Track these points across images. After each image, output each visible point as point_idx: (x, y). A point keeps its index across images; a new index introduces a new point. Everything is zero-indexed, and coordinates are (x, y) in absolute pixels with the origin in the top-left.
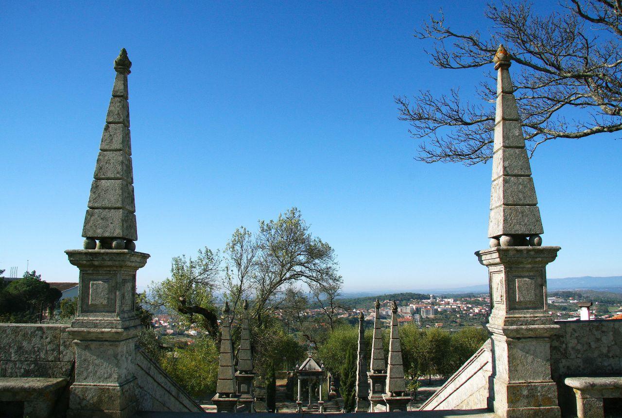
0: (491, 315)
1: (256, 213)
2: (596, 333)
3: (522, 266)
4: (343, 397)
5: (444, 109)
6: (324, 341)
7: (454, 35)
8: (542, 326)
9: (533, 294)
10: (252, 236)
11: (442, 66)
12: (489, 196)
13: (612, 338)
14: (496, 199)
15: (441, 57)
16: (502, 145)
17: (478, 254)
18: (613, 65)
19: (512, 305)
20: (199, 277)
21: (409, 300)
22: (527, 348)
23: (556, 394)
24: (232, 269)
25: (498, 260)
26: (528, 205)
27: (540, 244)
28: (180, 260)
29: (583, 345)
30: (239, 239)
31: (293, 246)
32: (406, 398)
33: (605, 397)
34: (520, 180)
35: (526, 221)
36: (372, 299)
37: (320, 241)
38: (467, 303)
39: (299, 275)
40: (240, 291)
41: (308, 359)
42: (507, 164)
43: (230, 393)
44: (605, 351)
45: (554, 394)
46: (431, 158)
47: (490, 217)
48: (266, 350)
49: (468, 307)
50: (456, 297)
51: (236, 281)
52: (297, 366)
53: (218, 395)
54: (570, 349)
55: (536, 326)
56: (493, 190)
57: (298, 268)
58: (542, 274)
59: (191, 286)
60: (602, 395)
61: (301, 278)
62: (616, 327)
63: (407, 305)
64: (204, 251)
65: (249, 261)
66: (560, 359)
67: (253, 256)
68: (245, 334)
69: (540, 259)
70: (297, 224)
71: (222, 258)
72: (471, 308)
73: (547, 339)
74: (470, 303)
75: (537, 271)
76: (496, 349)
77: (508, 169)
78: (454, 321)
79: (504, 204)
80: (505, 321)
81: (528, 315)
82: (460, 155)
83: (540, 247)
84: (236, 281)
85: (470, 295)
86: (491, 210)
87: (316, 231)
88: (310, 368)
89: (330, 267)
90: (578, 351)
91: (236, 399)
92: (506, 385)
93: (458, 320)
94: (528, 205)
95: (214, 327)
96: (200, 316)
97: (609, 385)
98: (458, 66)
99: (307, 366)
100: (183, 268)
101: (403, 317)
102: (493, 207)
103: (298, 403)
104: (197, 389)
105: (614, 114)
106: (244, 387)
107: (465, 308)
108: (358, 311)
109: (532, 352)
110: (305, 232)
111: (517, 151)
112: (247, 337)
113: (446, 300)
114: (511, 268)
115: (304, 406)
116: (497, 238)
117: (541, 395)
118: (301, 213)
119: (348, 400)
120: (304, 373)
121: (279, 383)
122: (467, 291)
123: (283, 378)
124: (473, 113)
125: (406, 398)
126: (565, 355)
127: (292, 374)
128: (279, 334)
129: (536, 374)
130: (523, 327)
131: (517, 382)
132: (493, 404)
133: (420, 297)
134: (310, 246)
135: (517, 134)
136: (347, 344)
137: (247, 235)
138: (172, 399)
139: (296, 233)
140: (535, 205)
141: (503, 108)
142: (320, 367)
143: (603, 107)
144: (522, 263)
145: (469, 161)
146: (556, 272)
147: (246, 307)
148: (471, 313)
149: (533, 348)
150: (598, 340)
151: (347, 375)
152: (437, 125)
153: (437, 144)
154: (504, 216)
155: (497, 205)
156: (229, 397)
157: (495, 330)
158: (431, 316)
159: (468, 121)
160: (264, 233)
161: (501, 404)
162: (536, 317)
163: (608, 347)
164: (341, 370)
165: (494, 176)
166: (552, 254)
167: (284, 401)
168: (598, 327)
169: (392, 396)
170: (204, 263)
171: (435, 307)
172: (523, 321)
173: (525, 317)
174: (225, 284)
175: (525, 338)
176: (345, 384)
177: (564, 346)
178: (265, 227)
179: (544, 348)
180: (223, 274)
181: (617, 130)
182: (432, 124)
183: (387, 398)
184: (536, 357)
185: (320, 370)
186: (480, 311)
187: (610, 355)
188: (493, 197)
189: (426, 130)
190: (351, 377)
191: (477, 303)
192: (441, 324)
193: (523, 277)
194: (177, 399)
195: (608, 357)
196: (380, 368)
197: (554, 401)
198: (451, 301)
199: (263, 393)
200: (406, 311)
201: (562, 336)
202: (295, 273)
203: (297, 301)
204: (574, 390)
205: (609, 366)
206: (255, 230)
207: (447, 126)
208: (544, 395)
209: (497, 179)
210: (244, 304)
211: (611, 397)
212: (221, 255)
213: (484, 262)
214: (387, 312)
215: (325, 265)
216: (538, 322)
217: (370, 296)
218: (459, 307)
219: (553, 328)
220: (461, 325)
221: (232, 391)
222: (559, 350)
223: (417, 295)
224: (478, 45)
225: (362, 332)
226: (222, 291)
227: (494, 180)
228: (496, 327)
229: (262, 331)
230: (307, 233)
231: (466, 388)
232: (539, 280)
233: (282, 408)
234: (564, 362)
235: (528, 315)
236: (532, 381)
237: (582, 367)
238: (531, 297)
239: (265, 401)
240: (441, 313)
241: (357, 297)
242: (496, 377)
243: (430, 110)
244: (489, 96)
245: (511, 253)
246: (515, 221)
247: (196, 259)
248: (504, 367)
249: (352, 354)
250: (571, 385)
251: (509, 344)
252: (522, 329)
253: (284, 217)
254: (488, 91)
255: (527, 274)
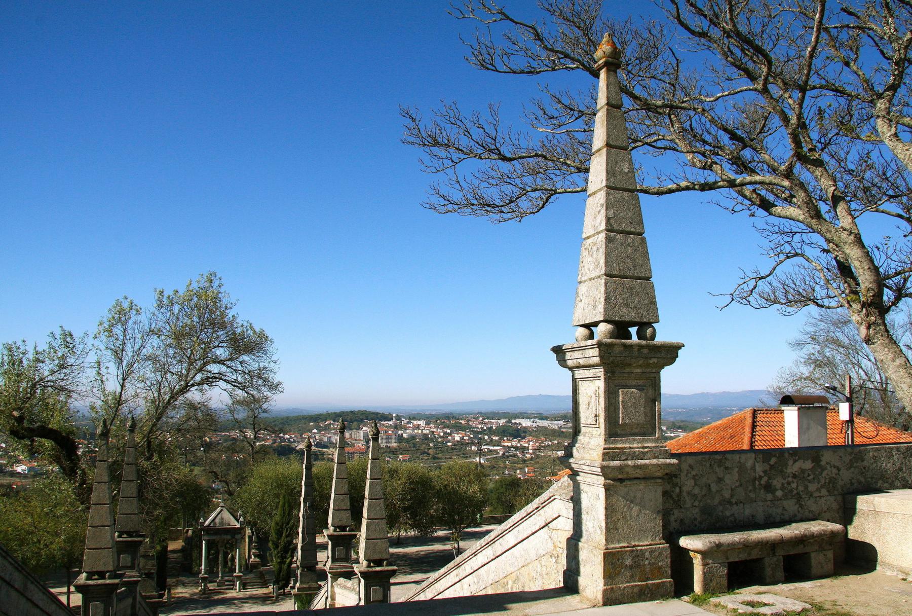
0: (577, 445)
1: (151, 280)
2: (717, 469)
3: (628, 370)
4: (273, 566)
5: (476, 133)
6: (241, 481)
7: (511, 20)
8: (655, 461)
9: (642, 413)
10: (143, 315)
11: (483, 66)
12: (575, 262)
13: (736, 476)
14: (592, 267)
15: (484, 51)
16: (604, 184)
17: (559, 351)
18: (712, 99)
19: (613, 430)
20: (50, 378)
21: (362, 421)
22: (632, 494)
23: (669, 560)
24: (107, 364)
25: (597, 360)
26: (640, 278)
27: (653, 337)
28: (18, 348)
29: (702, 488)
30: (122, 315)
31: (208, 332)
32: (390, 568)
33: (731, 560)
34: (630, 240)
35: (636, 302)
36: (336, 416)
37: (251, 328)
38: (444, 427)
39: (216, 378)
40: (119, 402)
41: (219, 509)
42: (611, 213)
43: (108, 572)
44: (727, 494)
45: (665, 562)
46: (450, 205)
47: (577, 294)
48: (161, 497)
49: (445, 433)
50: (430, 419)
51: (113, 386)
52: (201, 520)
53: (84, 575)
54: (685, 494)
55: (647, 461)
56: (585, 253)
57: (214, 368)
58: (655, 384)
59: (35, 392)
60: (727, 558)
61: (218, 384)
62: (742, 461)
63: (359, 428)
64: (58, 332)
65: (138, 353)
66: (671, 510)
67: (142, 346)
68: (128, 472)
69: (655, 360)
70: (216, 299)
71: (91, 347)
72: (450, 434)
73: (660, 481)
74: (448, 427)
75: (647, 378)
76: (584, 498)
77: (612, 221)
78: (425, 452)
79: (606, 275)
80: (604, 454)
81: (635, 445)
82: (487, 205)
83: (654, 342)
84: (113, 386)
85: (449, 416)
86: (580, 282)
87: (245, 312)
88: (222, 523)
89: (265, 368)
90: (694, 496)
91: (117, 581)
92: (602, 552)
93: (431, 451)
94: (640, 278)
95: (72, 461)
96: (47, 443)
97: (738, 543)
98: (505, 69)
99: (217, 520)
100: (21, 362)
101: (353, 445)
102: (585, 278)
103: (202, 578)
104: (34, 562)
105: (704, 168)
106: (125, 559)
107: (442, 434)
108: (287, 436)
109: (638, 501)
110: (228, 311)
111: (626, 195)
112: (133, 476)
113: (415, 422)
114: (613, 373)
115: (210, 582)
116: (589, 327)
117: (649, 564)
118: (223, 282)
119: (280, 569)
120: (213, 530)
121: (173, 546)
122: (446, 410)
123: (176, 539)
124: (515, 143)
125: (390, 568)
126: (678, 503)
127: (190, 533)
128: (180, 471)
129: (642, 533)
130: (630, 463)
131: (617, 545)
132: (577, 581)
133: (376, 418)
134: (234, 333)
135: (627, 170)
136: (281, 486)
137: (133, 312)
138: (14, 594)
139: (214, 313)
140: (648, 278)
141: (608, 129)
142: (238, 521)
143: (689, 157)
144: (630, 365)
145: (498, 216)
146: (674, 381)
147: (132, 429)
148: (449, 441)
149: (639, 495)
150: (720, 480)
151: (279, 533)
152: (462, 156)
153: (457, 186)
154: (606, 293)
155: (594, 275)
156: (104, 578)
157: (585, 467)
158: (394, 444)
159: (508, 155)
160: (163, 310)
161: (592, 578)
162: (647, 447)
163: (732, 490)
164: (271, 525)
165: (588, 231)
166: (670, 353)
167: (178, 576)
168: (720, 461)
169: (369, 566)
170: (60, 354)
171: (400, 432)
172: (629, 454)
173: (630, 448)
174: (95, 390)
175: (630, 479)
176: (277, 547)
177: (677, 490)
178: (165, 301)
179: (654, 494)
180: (91, 373)
181: (711, 189)
182: (456, 156)
183: (362, 569)
184: (644, 507)
185: (238, 526)
186: (462, 438)
187: (734, 501)
188: (585, 264)
189: (445, 161)
190: (287, 536)
191: (458, 428)
192: (407, 457)
193: (630, 387)
194: (22, 594)
195: (731, 504)
196: (344, 523)
197: (666, 572)
198: (422, 423)
199: (151, 565)
200: (359, 436)
201: (676, 476)
202: (209, 374)
203: (207, 419)
204: (691, 554)
205: (731, 515)
206: (147, 304)
207: (476, 161)
208: (654, 563)
209: (594, 235)
210: (129, 424)
211: (737, 560)
212: (90, 341)
213: (570, 363)
214: (329, 438)
215: (257, 365)
216: (649, 455)
217: (305, 414)
218: (433, 432)
219: (670, 464)
220: (434, 458)
221: (111, 568)
222: (671, 496)
223: (374, 413)
224: (541, 40)
225: (309, 468)
226: (88, 401)
227: (588, 238)
228: (589, 462)
229: (155, 467)
230: (230, 314)
231: (517, 553)
232: (651, 392)
233: (176, 585)
234: (677, 514)
235: (635, 444)
236: (637, 543)
237: (699, 519)
238: (639, 417)
239: (152, 579)
240: (407, 440)
241: (286, 415)
242: (582, 540)
243: (453, 133)
244: (542, 120)
245: (617, 350)
246: (622, 301)
247: (46, 347)
248: (596, 523)
249: (289, 501)
250: (689, 547)
251: (607, 488)
252: (627, 466)
253: (195, 286)
254: (542, 113)
255: (634, 383)
